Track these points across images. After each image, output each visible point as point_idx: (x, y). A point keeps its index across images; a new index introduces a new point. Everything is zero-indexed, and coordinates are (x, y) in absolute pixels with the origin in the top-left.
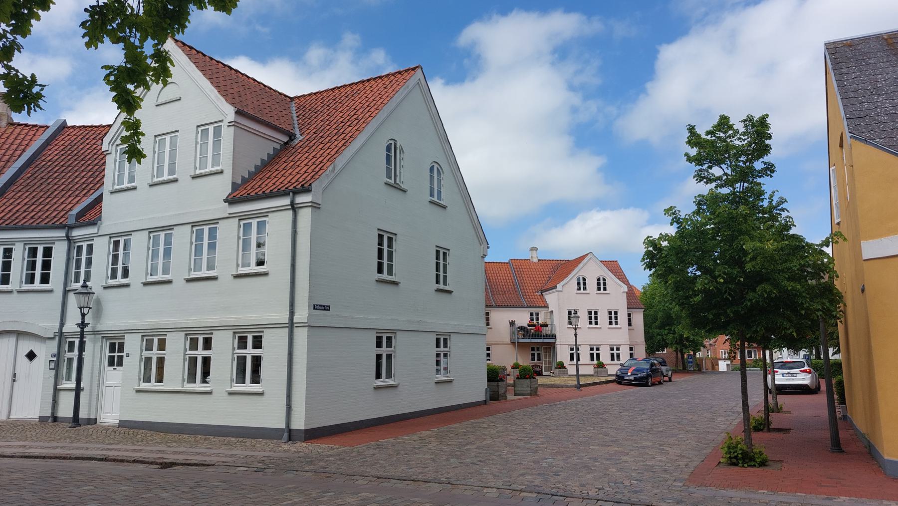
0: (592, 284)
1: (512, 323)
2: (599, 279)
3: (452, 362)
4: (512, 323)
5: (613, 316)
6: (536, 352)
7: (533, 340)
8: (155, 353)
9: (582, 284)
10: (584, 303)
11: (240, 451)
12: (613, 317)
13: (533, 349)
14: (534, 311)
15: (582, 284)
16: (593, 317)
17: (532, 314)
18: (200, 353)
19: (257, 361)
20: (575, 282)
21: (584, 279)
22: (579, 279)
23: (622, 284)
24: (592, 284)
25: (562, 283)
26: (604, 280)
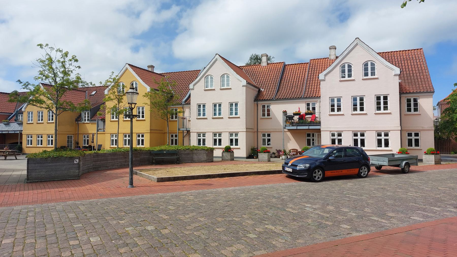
0: (357, 71)
1: (285, 112)
2: (366, 65)
3: (271, 142)
4: (285, 112)
5: (382, 101)
6: (311, 138)
7: (311, 127)
8: (30, 139)
9: (346, 72)
10: (347, 92)
11: (344, 172)
12: (382, 102)
13: (309, 135)
14: (308, 101)
15: (346, 72)
16: (217, 107)
17: (308, 105)
18: (40, 139)
19: (143, 140)
20: (338, 69)
21: (350, 66)
22: (343, 67)
23: (394, 67)
24: (357, 71)
25: (325, 72)
26: (373, 64)
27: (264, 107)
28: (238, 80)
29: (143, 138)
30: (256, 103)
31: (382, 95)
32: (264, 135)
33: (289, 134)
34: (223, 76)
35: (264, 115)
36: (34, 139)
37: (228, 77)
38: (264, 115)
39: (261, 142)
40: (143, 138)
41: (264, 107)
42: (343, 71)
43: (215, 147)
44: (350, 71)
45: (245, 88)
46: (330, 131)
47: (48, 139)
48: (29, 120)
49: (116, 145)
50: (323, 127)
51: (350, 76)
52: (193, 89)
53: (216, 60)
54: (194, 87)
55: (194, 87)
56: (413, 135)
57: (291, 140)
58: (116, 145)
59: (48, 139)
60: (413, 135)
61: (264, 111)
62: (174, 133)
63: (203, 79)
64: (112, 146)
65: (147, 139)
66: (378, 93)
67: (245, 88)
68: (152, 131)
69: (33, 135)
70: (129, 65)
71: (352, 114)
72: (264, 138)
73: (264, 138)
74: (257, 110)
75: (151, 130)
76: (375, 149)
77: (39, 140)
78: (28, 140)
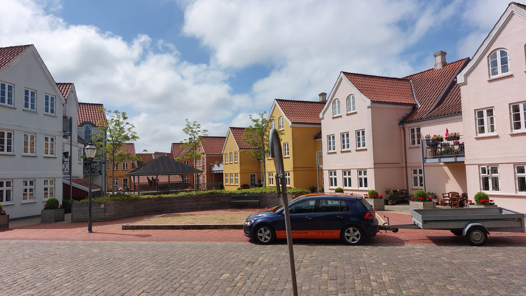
21: (503, 53)
22: (493, 55)
27: (413, 131)
28: (363, 100)
29: (8, 188)
30: (401, 126)
31: (521, 102)
32: (415, 172)
33: (446, 169)
34: (348, 98)
35: (414, 143)
36: (339, 177)
37: (353, 98)
38: (414, 143)
39: (411, 182)
40: (8, 188)
41: (413, 131)
42: (495, 64)
43: (345, 188)
44: (504, 61)
45: (370, 109)
46: (479, 165)
47: (345, 176)
48: (344, 146)
49: (421, 185)
50: (468, 158)
51: (505, 69)
52: (465, 84)
53: (341, 79)
54: (466, 80)
55: (466, 80)
56: (32, 187)
57: (449, 179)
58: (421, 185)
59: (345, 176)
60: (32, 187)
61: (413, 137)
62: (418, 167)
63: (485, 59)
64: (331, 187)
65: (371, 176)
66: (514, 100)
67: (370, 109)
68: (377, 165)
69: (337, 171)
70: (344, 73)
71: (512, 135)
72: (415, 175)
73: (415, 175)
74: (405, 136)
75: (375, 164)
76: (357, 189)
77: (361, 179)
78: (345, 179)
